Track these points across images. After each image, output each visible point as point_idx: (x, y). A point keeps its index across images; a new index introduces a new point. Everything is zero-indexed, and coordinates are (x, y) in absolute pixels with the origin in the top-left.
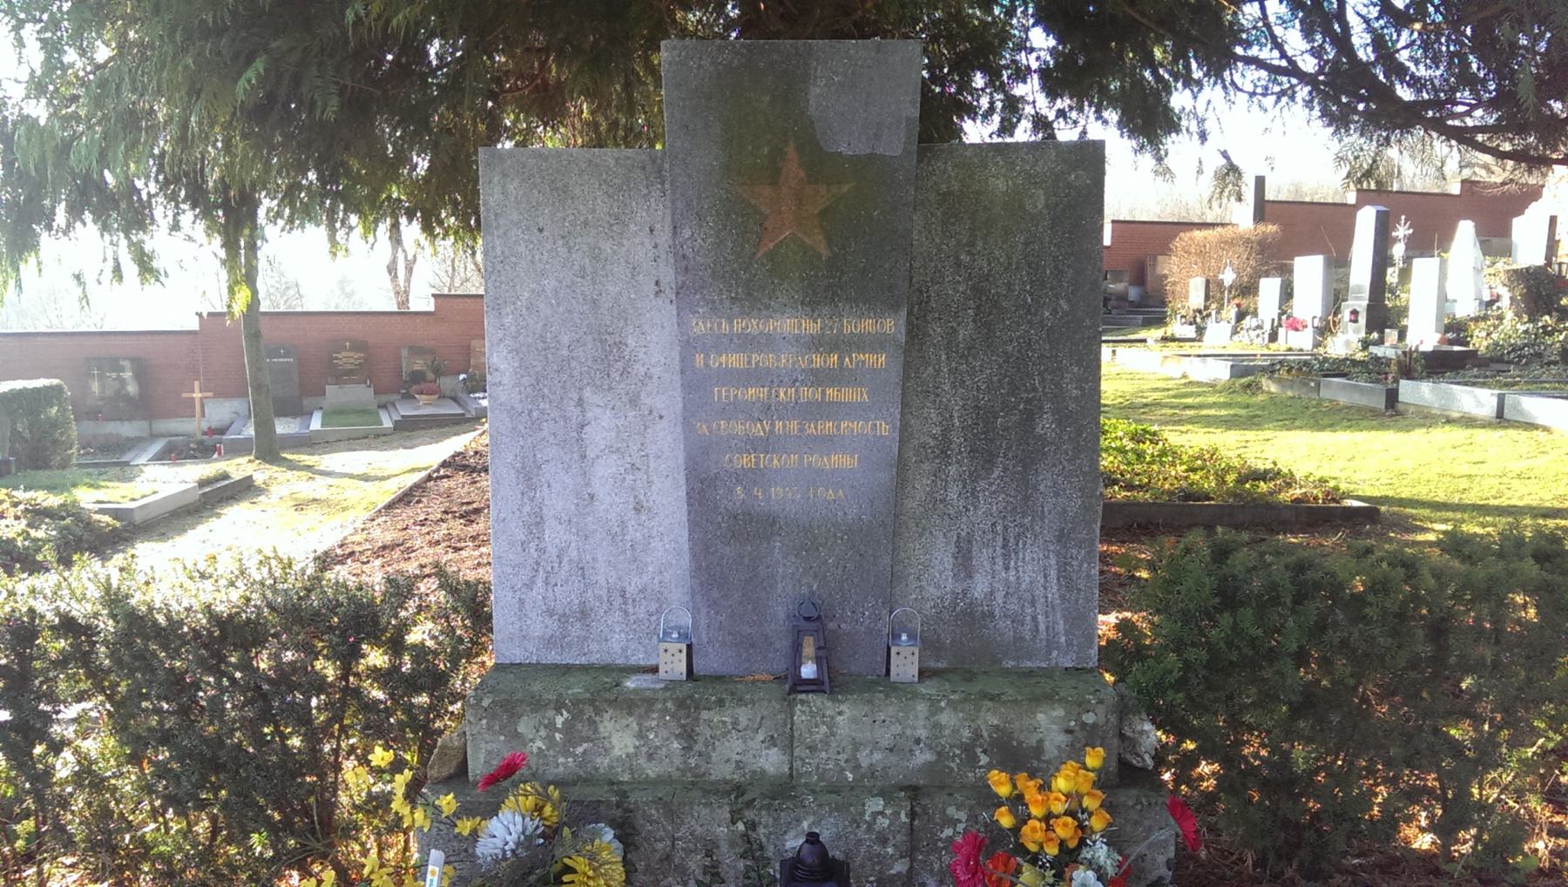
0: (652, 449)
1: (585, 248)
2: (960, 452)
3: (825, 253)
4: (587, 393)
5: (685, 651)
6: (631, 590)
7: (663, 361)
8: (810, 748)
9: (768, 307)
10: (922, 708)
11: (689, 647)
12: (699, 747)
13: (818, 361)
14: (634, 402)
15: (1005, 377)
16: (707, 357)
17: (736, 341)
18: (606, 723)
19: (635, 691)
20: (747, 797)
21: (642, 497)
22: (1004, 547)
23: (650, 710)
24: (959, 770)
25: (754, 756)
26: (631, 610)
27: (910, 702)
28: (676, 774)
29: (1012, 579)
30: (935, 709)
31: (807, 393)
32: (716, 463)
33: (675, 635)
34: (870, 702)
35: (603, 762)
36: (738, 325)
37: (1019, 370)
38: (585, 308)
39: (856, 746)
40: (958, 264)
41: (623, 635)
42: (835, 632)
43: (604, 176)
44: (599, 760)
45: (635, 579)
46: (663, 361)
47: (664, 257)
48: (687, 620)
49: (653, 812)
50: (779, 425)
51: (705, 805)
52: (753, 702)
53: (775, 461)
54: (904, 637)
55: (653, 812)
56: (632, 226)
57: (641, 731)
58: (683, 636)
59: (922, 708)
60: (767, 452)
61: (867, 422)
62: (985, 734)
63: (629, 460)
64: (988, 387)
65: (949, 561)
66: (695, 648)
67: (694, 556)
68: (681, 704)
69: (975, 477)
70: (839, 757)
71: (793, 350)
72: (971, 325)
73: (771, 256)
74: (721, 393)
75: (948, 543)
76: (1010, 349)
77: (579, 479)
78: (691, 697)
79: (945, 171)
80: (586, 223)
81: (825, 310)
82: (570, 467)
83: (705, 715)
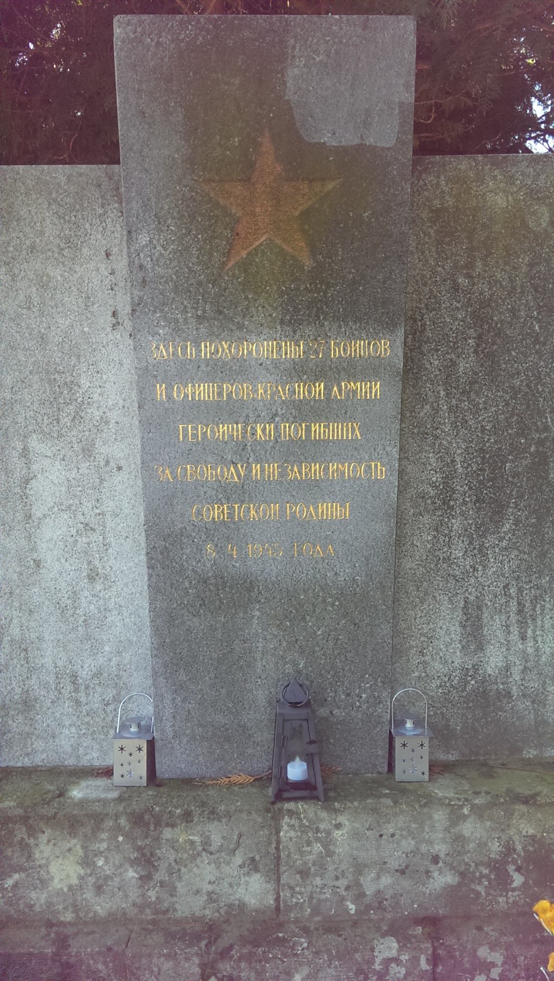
0: (109, 505)
1: (32, 276)
2: (465, 503)
3: (308, 263)
4: (34, 443)
5: (145, 749)
6: (84, 674)
7: (121, 403)
8: (301, 872)
9: (241, 327)
10: (440, 816)
11: (151, 744)
12: (161, 875)
13: (301, 391)
14: (88, 451)
15: (512, 415)
16: (169, 388)
17: (203, 367)
18: (42, 847)
19: (83, 803)
20: (223, 943)
21: (97, 563)
22: (520, 612)
23: (97, 828)
24: (488, 894)
25: (231, 885)
26: (83, 699)
27: (425, 810)
28: (132, 912)
29: (530, 650)
30: (456, 818)
31: (288, 430)
32: (182, 515)
33: (134, 729)
34: (375, 810)
35: (38, 898)
36: (207, 349)
37: (528, 406)
38: (31, 343)
39: (359, 868)
40: (456, 288)
41: (73, 730)
42: (326, 719)
43: (54, 195)
44: (33, 895)
45: (89, 661)
46: (121, 403)
47: (122, 284)
48: (147, 709)
49: (100, 966)
50: (256, 468)
51: (168, 957)
52: (228, 815)
53: (253, 512)
54: (409, 725)
55: (100, 966)
56: (85, 251)
57: (86, 856)
58: (144, 729)
59: (440, 816)
60: (243, 502)
61: (360, 463)
62: (519, 847)
63: (81, 518)
64: (494, 426)
65: (456, 630)
66: (158, 745)
67: (156, 631)
68: (138, 820)
69: (482, 530)
70: (338, 883)
71: (272, 378)
72: (472, 357)
73: (244, 266)
74: (187, 431)
75: (453, 610)
76: (517, 383)
77: (23, 542)
78: (149, 810)
79: (438, 185)
80: (33, 248)
81: (309, 330)
82: (11, 528)
83: (168, 833)
